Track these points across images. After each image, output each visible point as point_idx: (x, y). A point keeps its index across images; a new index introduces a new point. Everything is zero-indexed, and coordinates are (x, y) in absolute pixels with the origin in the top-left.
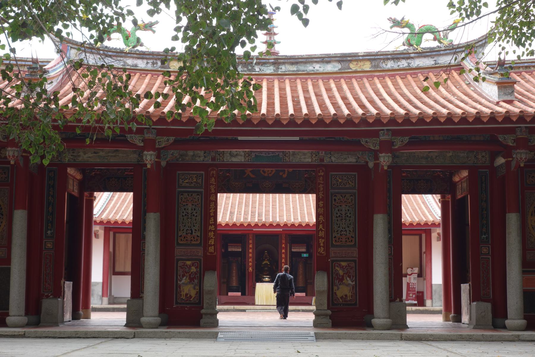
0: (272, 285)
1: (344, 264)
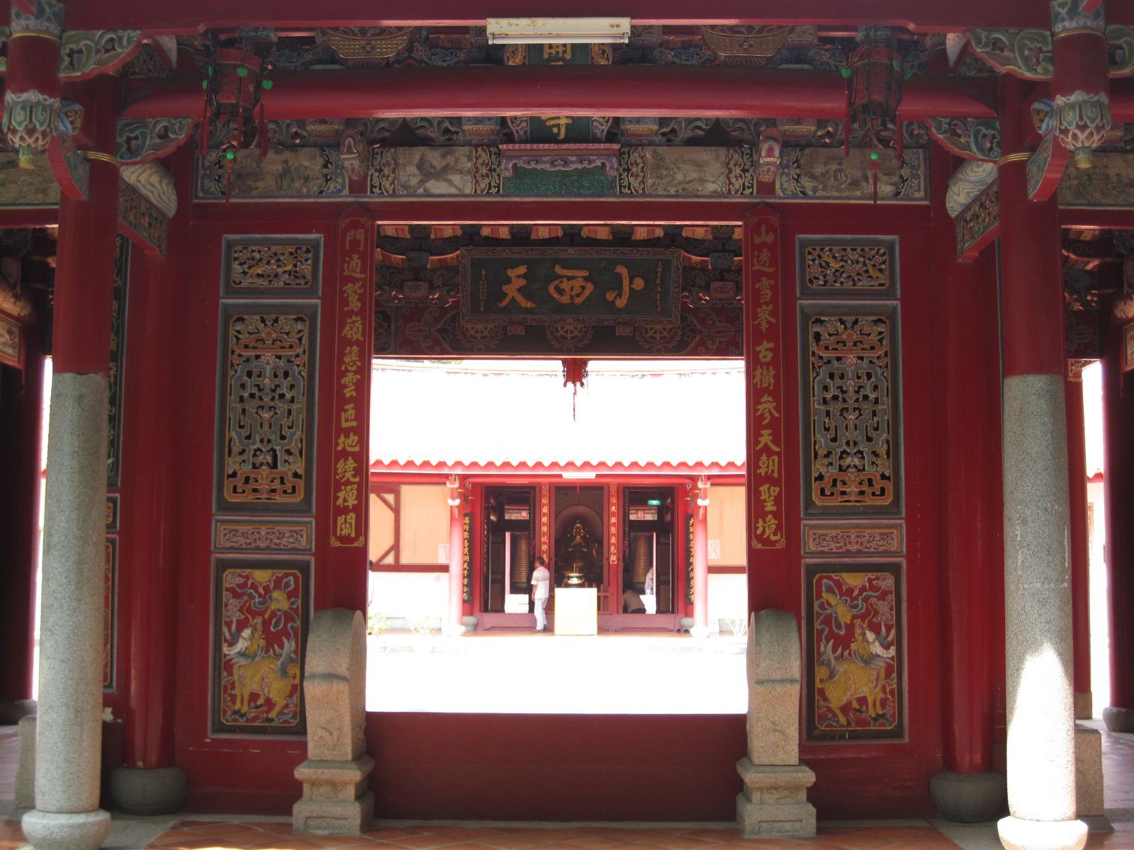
0: (592, 593)
1: (854, 580)
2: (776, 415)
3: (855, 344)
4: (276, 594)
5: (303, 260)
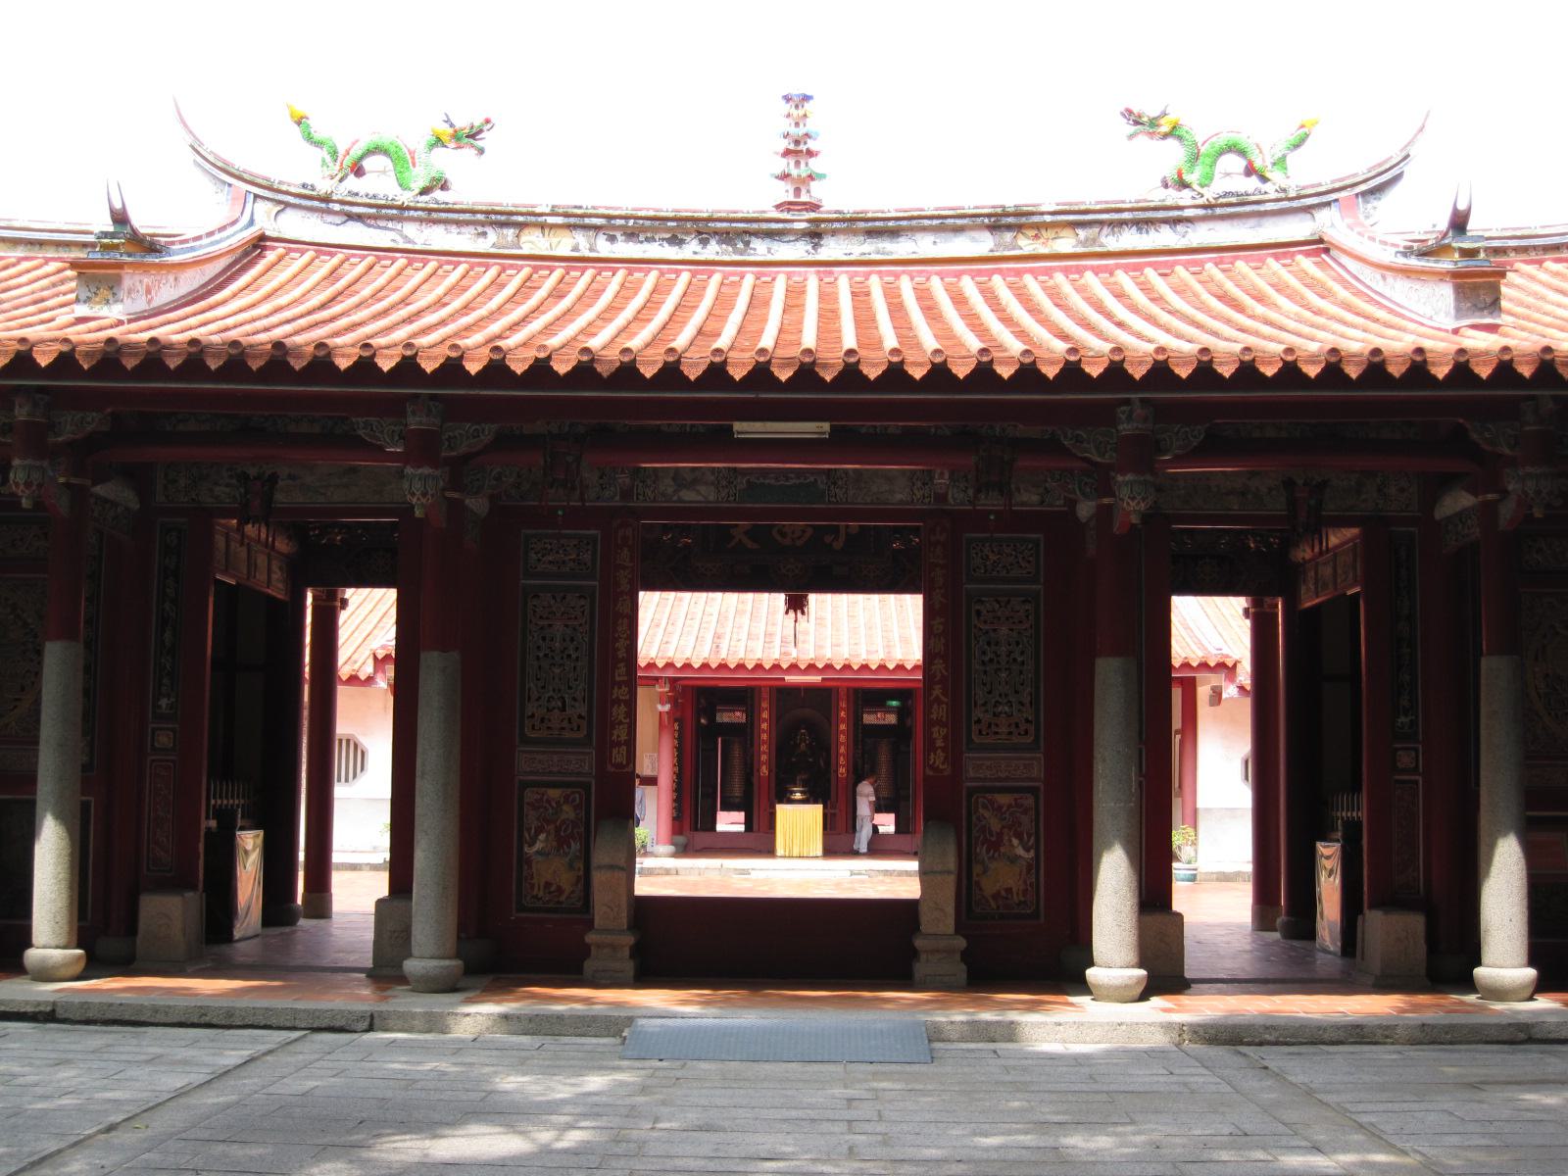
1: (1004, 799)
3: (1007, 619)
4: (565, 808)
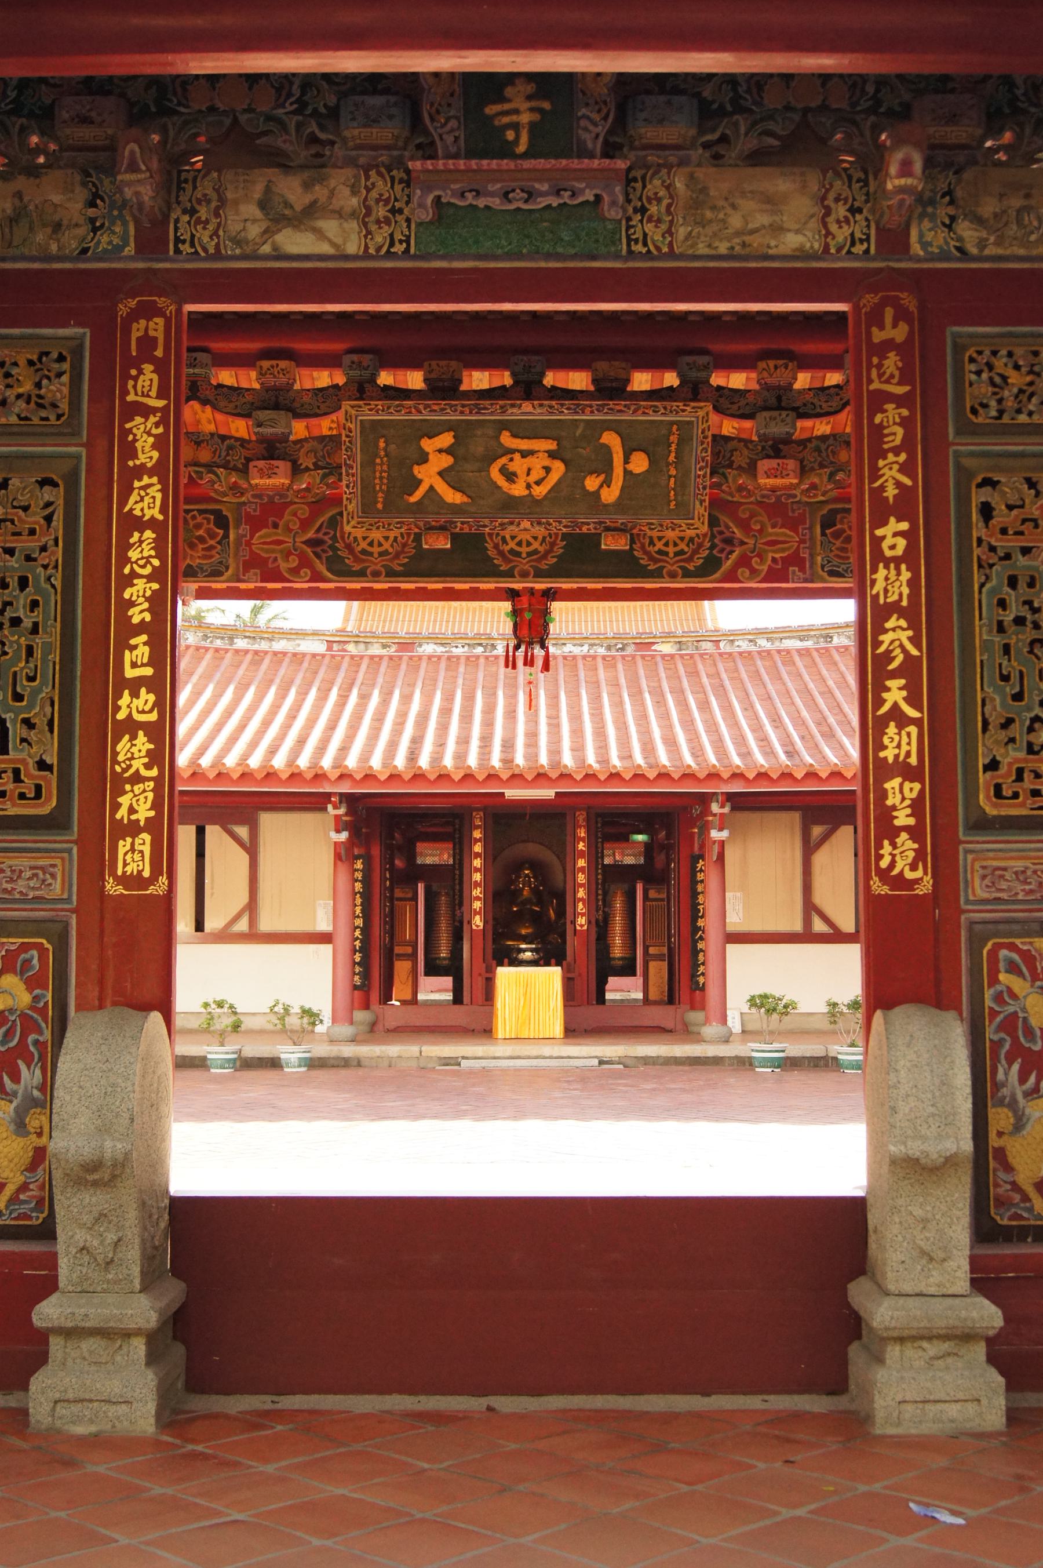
0: (553, 975)
2: (914, 652)
5: (52, 375)
